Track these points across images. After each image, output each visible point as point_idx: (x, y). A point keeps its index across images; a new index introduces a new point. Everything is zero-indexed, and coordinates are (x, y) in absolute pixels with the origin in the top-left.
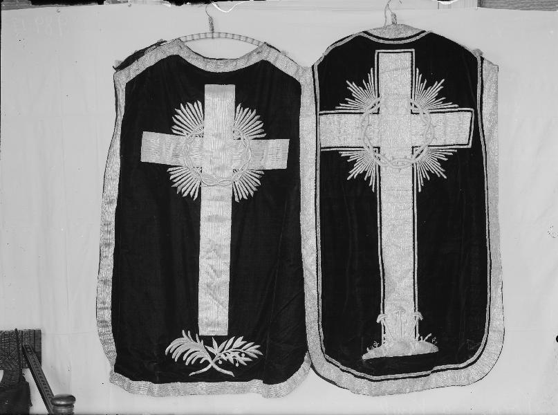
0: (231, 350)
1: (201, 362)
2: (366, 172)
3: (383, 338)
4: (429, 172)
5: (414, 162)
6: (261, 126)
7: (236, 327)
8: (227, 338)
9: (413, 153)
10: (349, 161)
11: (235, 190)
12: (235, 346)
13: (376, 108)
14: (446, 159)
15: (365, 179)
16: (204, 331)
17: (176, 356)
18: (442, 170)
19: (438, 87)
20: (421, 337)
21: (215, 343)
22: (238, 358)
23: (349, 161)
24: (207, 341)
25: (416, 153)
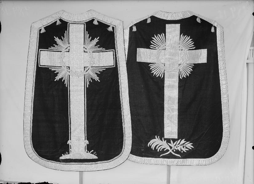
0: (179, 145)
1: (165, 150)
2: (63, 78)
3: (70, 151)
4: (92, 79)
5: (85, 74)
6: (193, 43)
7: (181, 135)
8: (178, 140)
9: (84, 70)
10: (55, 73)
11: (180, 73)
12: (181, 143)
13: (68, 49)
14: (99, 73)
15: (63, 81)
16: (166, 136)
17: (153, 147)
18: (58, 79)
19: (96, 40)
20: (88, 151)
21: (172, 142)
22: (183, 149)
23: (55, 73)
24: (168, 141)
25: (86, 70)
